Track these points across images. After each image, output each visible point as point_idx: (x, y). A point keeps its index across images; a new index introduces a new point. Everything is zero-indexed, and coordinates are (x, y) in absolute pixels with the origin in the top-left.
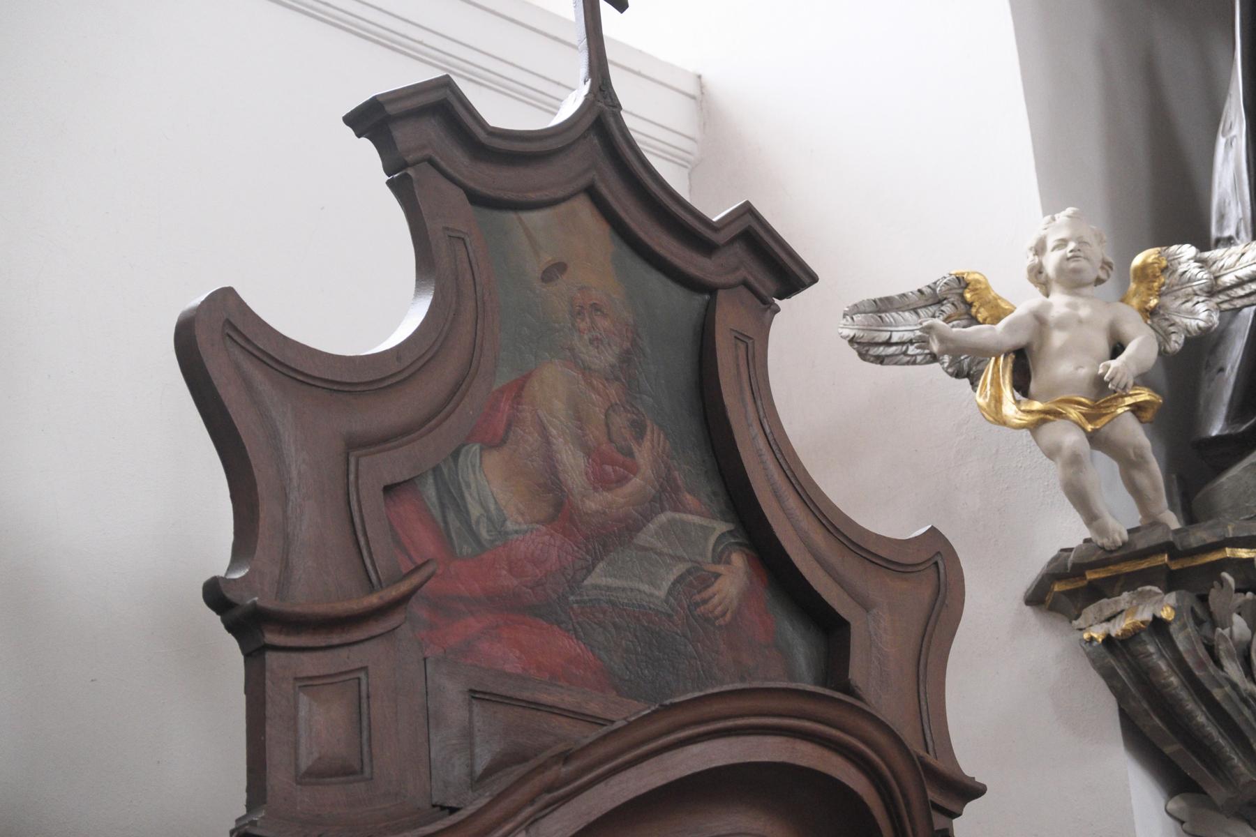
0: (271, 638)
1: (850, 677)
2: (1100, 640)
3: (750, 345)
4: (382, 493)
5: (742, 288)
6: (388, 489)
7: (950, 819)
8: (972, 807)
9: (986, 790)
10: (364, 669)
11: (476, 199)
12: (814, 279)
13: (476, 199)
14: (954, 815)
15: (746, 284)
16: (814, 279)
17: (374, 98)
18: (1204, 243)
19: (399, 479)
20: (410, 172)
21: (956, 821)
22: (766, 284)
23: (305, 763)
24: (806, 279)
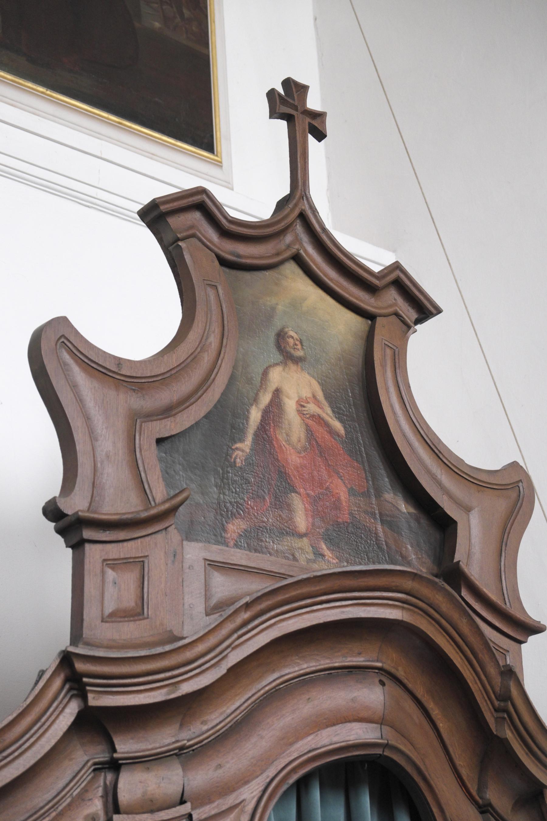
0: (87, 534)
1: (457, 557)
2: (202, 626)
3: (397, 352)
4: (155, 443)
5: (394, 317)
6: (160, 441)
7: (519, 645)
8: (532, 639)
9: (546, 627)
10: (521, 481)
11: (224, 262)
12: (439, 311)
13: (224, 262)
14: (520, 642)
15: (397, 314)
16: (439, 311)
17: (154, 200)
18: (283, 339)
19: (173, 433)
20: (180, 243)
21: (523, 646)
22: (411, 314)
23: (108, 611)
24: (434, 311)
